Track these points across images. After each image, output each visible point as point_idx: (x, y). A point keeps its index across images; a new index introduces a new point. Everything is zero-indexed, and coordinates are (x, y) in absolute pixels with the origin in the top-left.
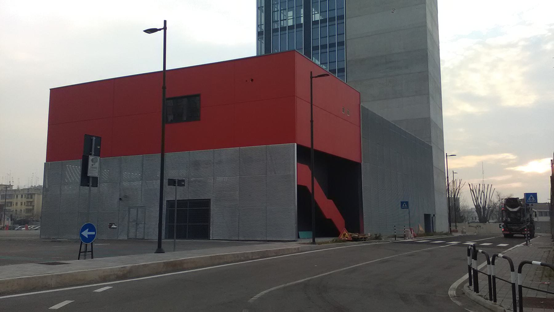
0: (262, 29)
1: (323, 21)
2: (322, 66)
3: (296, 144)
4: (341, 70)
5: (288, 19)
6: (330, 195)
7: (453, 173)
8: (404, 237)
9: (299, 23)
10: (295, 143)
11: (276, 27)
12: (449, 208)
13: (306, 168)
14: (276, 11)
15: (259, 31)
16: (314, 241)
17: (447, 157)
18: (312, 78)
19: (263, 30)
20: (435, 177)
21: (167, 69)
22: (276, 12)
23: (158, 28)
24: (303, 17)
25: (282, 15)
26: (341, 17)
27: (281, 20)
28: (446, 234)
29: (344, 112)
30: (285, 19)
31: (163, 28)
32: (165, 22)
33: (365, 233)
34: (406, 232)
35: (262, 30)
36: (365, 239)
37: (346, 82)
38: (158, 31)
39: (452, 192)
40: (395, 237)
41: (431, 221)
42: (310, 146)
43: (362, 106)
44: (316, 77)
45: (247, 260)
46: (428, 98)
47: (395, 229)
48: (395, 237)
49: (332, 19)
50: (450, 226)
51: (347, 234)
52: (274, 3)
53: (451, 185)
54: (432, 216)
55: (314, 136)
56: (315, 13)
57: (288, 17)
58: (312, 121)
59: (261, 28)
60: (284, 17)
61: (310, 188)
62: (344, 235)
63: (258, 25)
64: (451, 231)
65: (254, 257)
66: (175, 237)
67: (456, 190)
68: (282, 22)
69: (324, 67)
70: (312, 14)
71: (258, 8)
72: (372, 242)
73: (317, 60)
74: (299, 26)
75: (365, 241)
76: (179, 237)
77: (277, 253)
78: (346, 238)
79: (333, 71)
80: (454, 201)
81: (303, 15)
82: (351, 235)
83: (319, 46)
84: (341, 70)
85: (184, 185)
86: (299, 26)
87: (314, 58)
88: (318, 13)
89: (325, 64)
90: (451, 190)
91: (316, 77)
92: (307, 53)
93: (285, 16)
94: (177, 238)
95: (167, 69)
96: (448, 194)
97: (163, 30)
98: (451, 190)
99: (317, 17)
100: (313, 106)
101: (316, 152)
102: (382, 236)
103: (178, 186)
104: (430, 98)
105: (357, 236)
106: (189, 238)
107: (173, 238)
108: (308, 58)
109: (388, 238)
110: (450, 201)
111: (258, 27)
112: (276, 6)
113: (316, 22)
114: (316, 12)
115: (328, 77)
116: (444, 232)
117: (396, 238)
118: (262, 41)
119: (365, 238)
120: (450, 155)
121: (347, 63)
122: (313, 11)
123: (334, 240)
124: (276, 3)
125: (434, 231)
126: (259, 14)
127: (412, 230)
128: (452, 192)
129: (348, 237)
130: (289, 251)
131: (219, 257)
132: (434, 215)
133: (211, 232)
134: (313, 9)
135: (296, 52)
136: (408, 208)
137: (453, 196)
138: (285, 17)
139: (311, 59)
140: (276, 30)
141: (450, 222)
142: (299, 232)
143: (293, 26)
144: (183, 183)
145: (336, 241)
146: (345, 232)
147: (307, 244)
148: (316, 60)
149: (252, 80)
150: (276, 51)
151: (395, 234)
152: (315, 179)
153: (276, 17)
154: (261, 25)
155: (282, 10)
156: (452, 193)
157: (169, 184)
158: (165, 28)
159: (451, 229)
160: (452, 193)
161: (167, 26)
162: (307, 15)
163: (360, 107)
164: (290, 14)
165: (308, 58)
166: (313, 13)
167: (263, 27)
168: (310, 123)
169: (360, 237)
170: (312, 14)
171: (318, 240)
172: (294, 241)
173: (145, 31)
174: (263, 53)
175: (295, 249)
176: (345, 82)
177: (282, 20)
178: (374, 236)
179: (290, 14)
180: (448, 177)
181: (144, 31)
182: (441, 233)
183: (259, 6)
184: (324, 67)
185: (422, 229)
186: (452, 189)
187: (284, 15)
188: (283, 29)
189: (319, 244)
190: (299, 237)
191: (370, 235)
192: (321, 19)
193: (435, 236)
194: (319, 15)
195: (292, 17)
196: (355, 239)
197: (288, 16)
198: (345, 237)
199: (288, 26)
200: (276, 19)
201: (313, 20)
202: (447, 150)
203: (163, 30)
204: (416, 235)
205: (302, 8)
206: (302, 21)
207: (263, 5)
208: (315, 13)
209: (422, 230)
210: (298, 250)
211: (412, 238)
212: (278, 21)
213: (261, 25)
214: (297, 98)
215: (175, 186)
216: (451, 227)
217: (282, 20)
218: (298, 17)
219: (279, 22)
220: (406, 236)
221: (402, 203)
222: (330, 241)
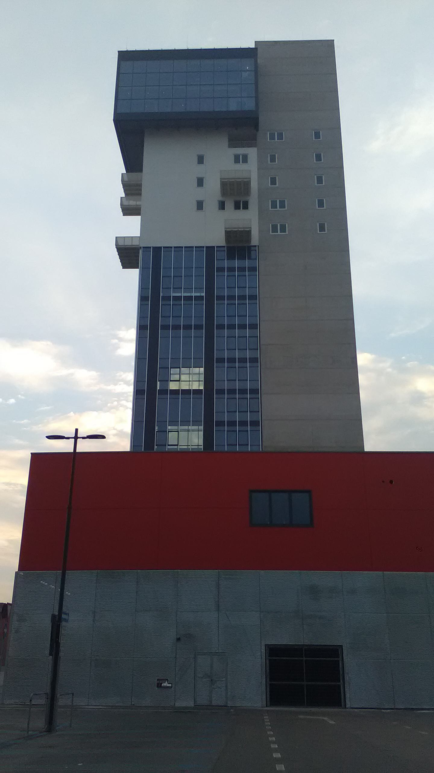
21: (77, 451)
95: (77, 451)
205: (193, 293)
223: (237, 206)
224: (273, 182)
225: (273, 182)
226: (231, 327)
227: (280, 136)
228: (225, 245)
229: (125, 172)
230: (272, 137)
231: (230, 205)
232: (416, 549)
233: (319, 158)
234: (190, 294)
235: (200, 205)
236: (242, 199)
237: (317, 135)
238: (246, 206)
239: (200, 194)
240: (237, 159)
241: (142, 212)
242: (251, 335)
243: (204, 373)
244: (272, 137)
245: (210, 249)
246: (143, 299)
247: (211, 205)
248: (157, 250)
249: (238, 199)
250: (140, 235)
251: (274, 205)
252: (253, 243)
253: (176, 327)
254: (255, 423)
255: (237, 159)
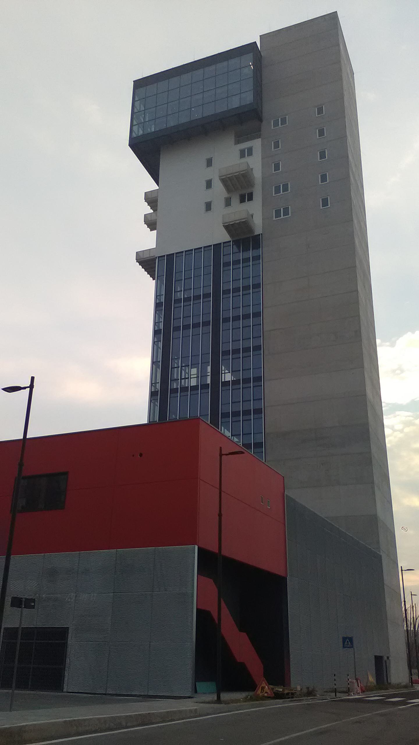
0: (157, 389)
1: (235, 382)
2: (234, 439)
3: (196, 547)
4: (258, 445)
5: (191, 378)
6: (242, 625)
7: (412, 595)
8: (348, 692)
9: (206, 383)
10: (196, 545)
11: (175, 387)
12: (408, 645)
13: (210, 583)
14: (176, 368)
15: (155, 329)
16: (219, 697)
17: (403, 571)
18: (221, 455)
19: (158, 389)
20: (388, 600)
21: (28, 437)
22: (176, 369)
23: (22, 386)
24: (210, 376)
25: (183, 372)
26: (258, 379)
27: (181, 379)
28: (406, 687)
29: (263, 503)
30: (187, 377)
31: (29, 386)
32: (33, 378)
33: (293, 685)
34: (350, 683)
35: (157, 390)
36: (291, 696)
37: (265, 462)
38: (22, 390)
39: (410, 622)
40: (335, 691)
41: (385, 668)
42: (215, 550)
43: (286, 495)
44: (227, 455)
45: (119, 729)
46: (373, 488)
47: (335, 680)
48: (335, 691)
49: (246, 381)
50: (411, 674)
51: (266, 687)
52: (173, 358)
53: (409, 612)
54: (385, 658)
55: (222, 504)
56: (225, 371)
57: (191, 375)
58: (220, 515)
59: (159, 327)
60: (185, 375)
61: (215, 615)
62: (263, 688)
63: (155, 323)
64: (412, 682)
65: (129, 724)
66: (14, 685)
67: (416, 619)
68: (183, 381)
69: (236, 440)
70: (222, 374)
71: (153, 363)
72: (303, 700)
73: (227, 430)
74: (205, 386)
75: (292, 698)
76: (19, 687)
77: (166, 717)
78: (266, 694)
79: (248, 446)
80: (414, 636)
81: (210, 374)
82: (273, 689)
83: (230, 412)
84: (258, 445)
85: (33, 607)
86: (205, 386)
87: (223, 428)
88: (230, 372)
89: (238, 435)
90: (409, 620)
91: (227, 455)
92: (215, 422)
93: (187, 373)
94: (18, 687)
95: (28, 437)
96: (405, 626)
97: (29, 389)
98: (409, 620)
99: (228, 377)
100: (223, 494)
101: (225, 558)
102: (317, 691)
103: (24, 607)
104: (376, 488)
105: (281, 690)
106: (34, 688)
107: (9, 686)
108: (215, 428)
109: (326, 693)
110: (409, 637)
111: (154, 344)
112: (176, 361)
113: (226, 384)
114: (227, 371)
115: (241, 455)
116: (403, 684)
117: (337, 694)
118: (156, 403)
119: (292, 694)
120: (406, 569)
121: (266, 436)
122: (223, 369)
123: (247, 697)
124: (176, 358)
125: (389, 682)
126: (158, 285)
127: (359, 681)
128: (410, 622)
129: (268, 691)
130: (181, 714)
131: (78, 723)
132: (388, 658)
133: (66, 679)
134: (223, 367)
135: (200, 420)
136: (352, 647)
137: (412, 629)
138: (187, 375)
139: (219, 429)
140: (175, 391)
141: (410, 667)
142: (196, 683)
143: (198, 386)
144: (33, 604)
145: (252, 699)
146: (264, 685)
147: (209, 703)
148: (225, 430)
149: (141, 455)
150: (174, 416)
151: (335, 687)
152: (223, 604)
153: (176, 374)
154: (156, 383)
155: (183, 366)
156: (411, 625)
157: (13, 605)
158: (31, 387)
159: (411, 678)
160: (411, 625)
161: (34, 384)
162: (216, 373)
163: (284, 496)
164: (194, 371)
165: (215, 428)
166: (223, 372)
167: (158, 386)
168: (218, 518)
169: (286, 692)
170: (222, 374)
171: (225, 696)
172: (189, 697)
173: (5, 389)
174: (157, 419)
175: (191, 711)
176: (264, 461)
177: (183, 379)
178: (305, 690)
179: (194, 371)
180: (405, 601)
181: (3, 389)
182: (398, 684)
183: (153, 382)
184: (236, 440)
185: (372, 679)
186: (411, 618)
187: (185, 373)
188: (184, 389)
189: (227, 703)
190: (196, 692)
191: (300, 690)
192: (232, 379)
193: (391, 690)
194: (230, 374)
195: (196, 376)
196: (278, 696)
197: (191, 374)
198: (264, 692)
199: (190, 386)
200: (175, 377)
201: (223, 381)
202: (402, 563)
203: (29, 389)
204: (364, 689)
205: (209, 366)
206: (209, 381)
207: (159, 380)
208: (225, 371)
209: (373, 680)
210: (196, 713)
211: (359, 693)
212: (179, 379)
213: (156, 383)
214: (200, 481)
215: (21, 607)
216: (411, 675)
217: (183, 379)
218: (204, 376)
219: (179, 381)
220: (350, 690)
221: (344, 639)
222: (243, 699)
223: (242, 200)
224: (277, 167)
225: (277, 167)
226: (236, 318)
227: (284, 121)
228: (230, 240)
229: (156, 231)
230: (276, 124)
231: (235, 200)
232: (402, 529)
233: (321, 133)
234: (210, 371)
235: (208, 206)
236: (246, 191)
237: (320, 111)
238: (250, 197)
239: (207, 196)
240: (242, 154)
241: (158, 226)
242: (239, 403)
243: (211, 371)
244: (276, 124)
245: (217, 246)
246: (158, 305)
247: (218, 205)
248: (170, 257)
249: (243, 192)
250: (156, 246)
251: (277, 190)
252: (256, 233)
253: (186, 327)
254: (258, 411)
255: (242, 154)
